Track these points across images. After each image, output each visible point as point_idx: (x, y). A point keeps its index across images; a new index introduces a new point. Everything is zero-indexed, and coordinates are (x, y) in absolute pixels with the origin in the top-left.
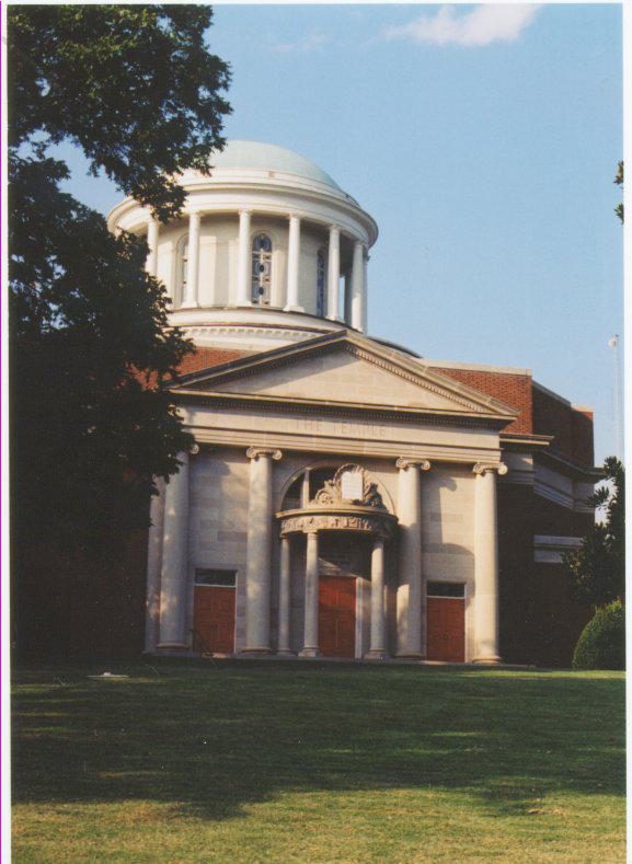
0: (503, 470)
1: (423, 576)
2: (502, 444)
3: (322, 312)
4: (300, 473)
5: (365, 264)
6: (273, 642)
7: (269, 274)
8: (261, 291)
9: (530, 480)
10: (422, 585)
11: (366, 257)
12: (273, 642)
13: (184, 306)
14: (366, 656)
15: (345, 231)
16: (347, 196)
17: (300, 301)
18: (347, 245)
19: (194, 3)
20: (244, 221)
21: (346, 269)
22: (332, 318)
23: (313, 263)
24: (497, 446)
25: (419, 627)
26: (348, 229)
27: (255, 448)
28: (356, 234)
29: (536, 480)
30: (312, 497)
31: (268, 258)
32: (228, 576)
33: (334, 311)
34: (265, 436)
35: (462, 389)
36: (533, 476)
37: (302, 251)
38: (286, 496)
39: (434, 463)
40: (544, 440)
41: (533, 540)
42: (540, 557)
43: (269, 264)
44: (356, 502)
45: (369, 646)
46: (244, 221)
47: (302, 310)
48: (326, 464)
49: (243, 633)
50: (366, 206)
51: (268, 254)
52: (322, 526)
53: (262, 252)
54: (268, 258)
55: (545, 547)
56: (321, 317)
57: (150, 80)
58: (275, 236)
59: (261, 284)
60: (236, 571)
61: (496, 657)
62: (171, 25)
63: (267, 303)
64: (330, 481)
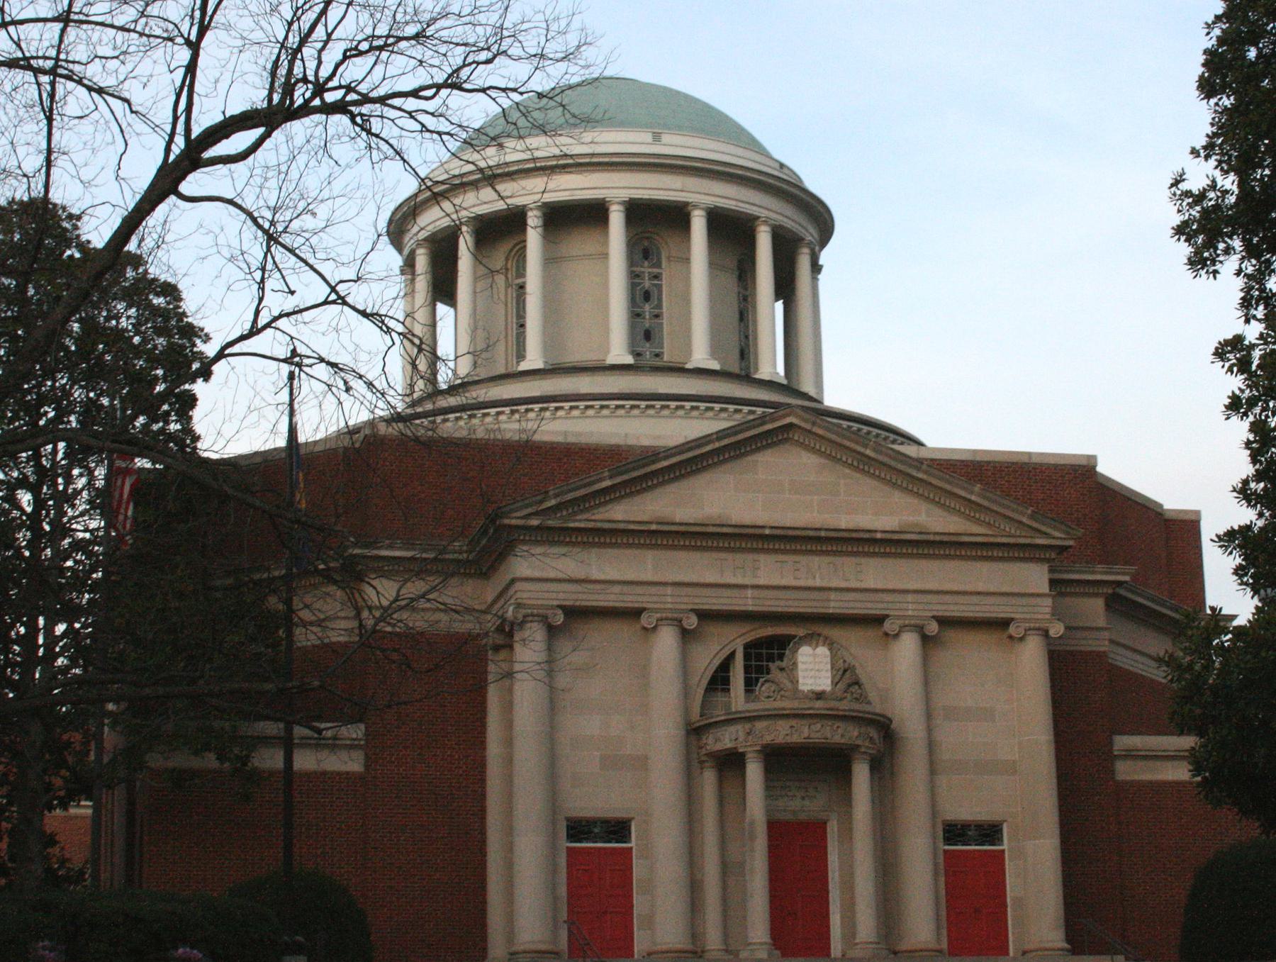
0: (1057, 630)
1: (934, 814)
2: (1053, 582)
3: (748, 368)
4: (726, 652)
5: (815, 279)
6: (695, 934)
7: (659, 306)
8: (647, 296)
9: (1098, 643)
10: (934, 826)
11: (816, 268)
12: (695, 934)
13: (524, 366)
14: (851, 954)
15: (781, 227)
16: (782, 166)
17: (715, 351)
18: (786, 248)
19: (244, 109)
20: (617, 219)
21: (785, 288)
22: (764, 373)
23: (729, 281)
24: (1045, 588)
25: (931, 867)
26: (789, 224)
27: (657, 610)
28: (801, 231)
29: (1112, 641)
30: (750, 684)
31: (657, 316)
32: (618, 829)
33: (773, 364)
34: (669, 590)
35: (984, 498)
36: (1106, 634)
37: (712, 265)
38: (707, 690)
39: (944, 622)
40: (1123, 574)
41: (1111, 743)
42: (1126, 771)
43: (659, 287)
44: (819, 695)
45: (854, 935)
46: (617, 219)
47: (715, 365)
48: (769, 631)
49: (650, 922)
50: (814, 184)
51: (656, 270)
52: (768, 739)
53: (646, 269)
54: (657, 316)
55: (1131, 755)
56: (746, 377)
57: (82, 555)
58: (667, 246)
59: (647, 284)
60: (633, 818)
61: (1066, 946)
62: (79, 328)
63: (657, 355)
64: (778, 663)
